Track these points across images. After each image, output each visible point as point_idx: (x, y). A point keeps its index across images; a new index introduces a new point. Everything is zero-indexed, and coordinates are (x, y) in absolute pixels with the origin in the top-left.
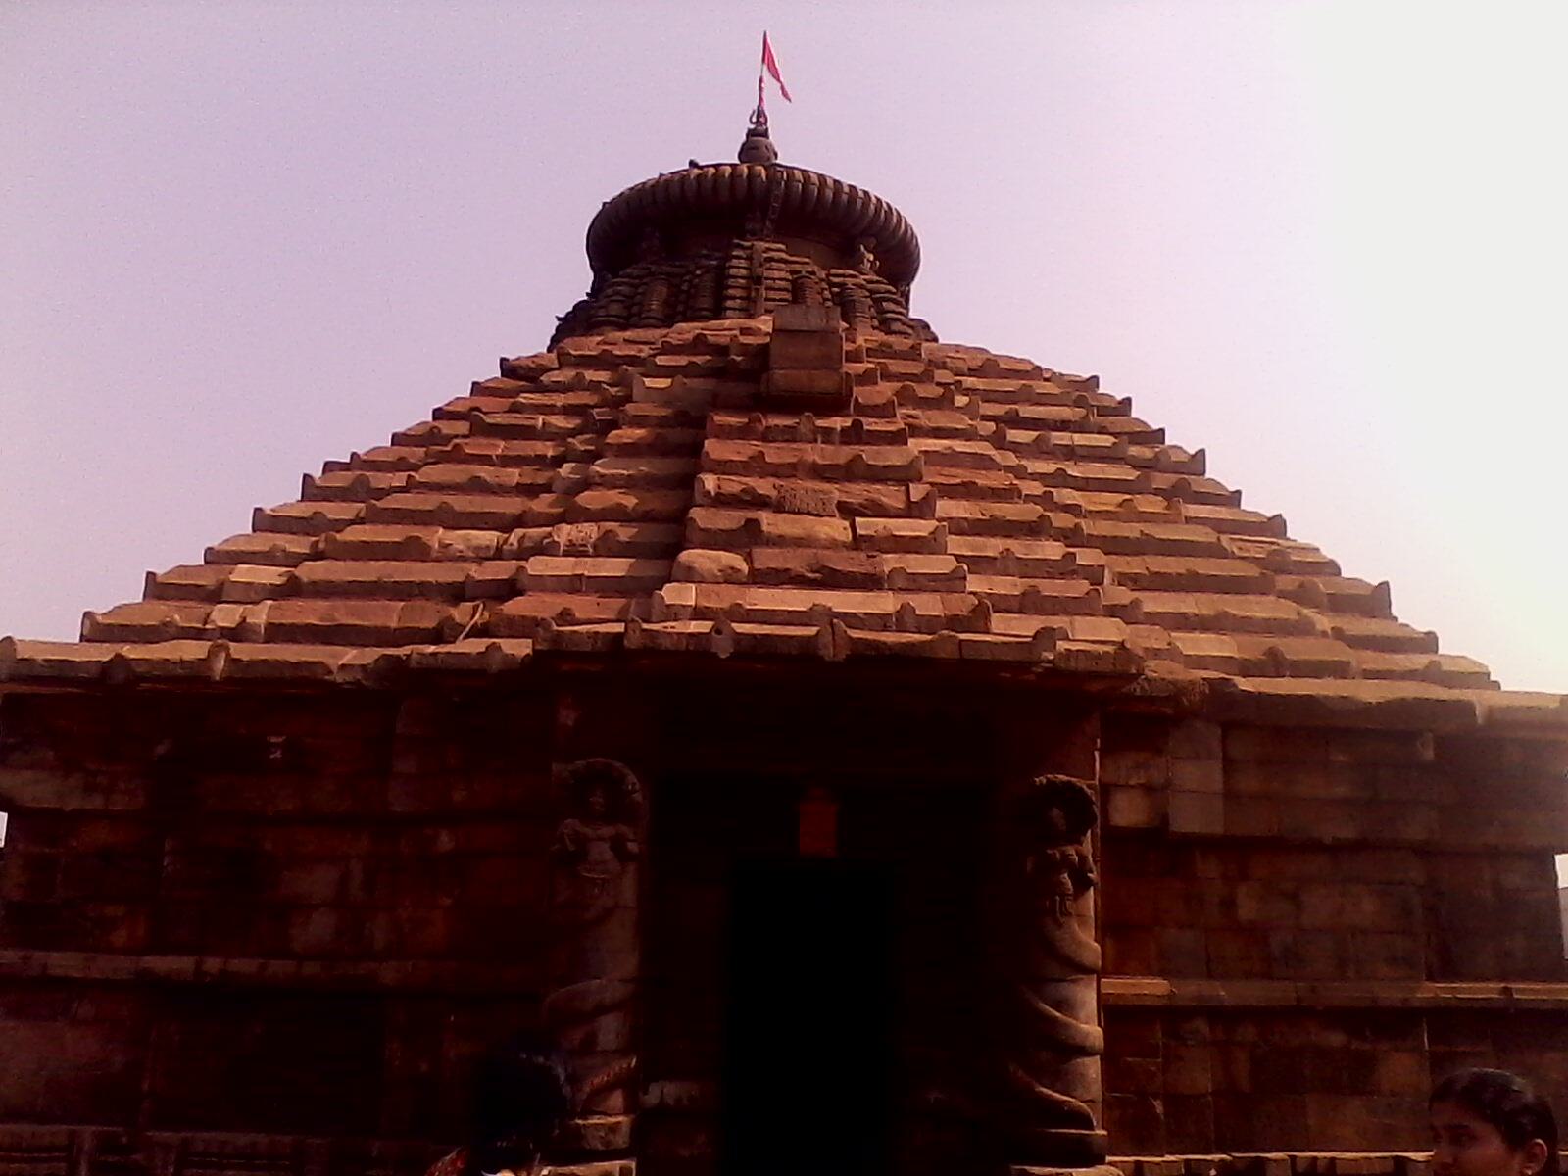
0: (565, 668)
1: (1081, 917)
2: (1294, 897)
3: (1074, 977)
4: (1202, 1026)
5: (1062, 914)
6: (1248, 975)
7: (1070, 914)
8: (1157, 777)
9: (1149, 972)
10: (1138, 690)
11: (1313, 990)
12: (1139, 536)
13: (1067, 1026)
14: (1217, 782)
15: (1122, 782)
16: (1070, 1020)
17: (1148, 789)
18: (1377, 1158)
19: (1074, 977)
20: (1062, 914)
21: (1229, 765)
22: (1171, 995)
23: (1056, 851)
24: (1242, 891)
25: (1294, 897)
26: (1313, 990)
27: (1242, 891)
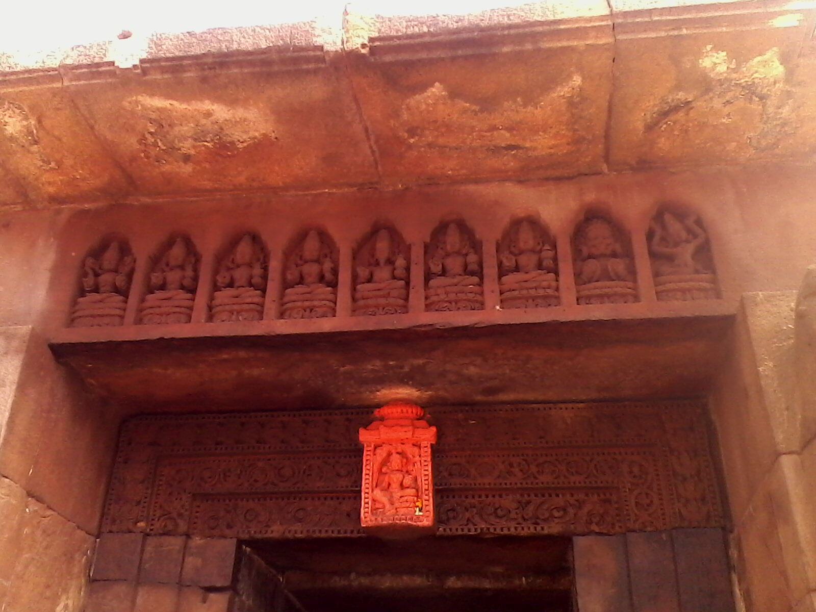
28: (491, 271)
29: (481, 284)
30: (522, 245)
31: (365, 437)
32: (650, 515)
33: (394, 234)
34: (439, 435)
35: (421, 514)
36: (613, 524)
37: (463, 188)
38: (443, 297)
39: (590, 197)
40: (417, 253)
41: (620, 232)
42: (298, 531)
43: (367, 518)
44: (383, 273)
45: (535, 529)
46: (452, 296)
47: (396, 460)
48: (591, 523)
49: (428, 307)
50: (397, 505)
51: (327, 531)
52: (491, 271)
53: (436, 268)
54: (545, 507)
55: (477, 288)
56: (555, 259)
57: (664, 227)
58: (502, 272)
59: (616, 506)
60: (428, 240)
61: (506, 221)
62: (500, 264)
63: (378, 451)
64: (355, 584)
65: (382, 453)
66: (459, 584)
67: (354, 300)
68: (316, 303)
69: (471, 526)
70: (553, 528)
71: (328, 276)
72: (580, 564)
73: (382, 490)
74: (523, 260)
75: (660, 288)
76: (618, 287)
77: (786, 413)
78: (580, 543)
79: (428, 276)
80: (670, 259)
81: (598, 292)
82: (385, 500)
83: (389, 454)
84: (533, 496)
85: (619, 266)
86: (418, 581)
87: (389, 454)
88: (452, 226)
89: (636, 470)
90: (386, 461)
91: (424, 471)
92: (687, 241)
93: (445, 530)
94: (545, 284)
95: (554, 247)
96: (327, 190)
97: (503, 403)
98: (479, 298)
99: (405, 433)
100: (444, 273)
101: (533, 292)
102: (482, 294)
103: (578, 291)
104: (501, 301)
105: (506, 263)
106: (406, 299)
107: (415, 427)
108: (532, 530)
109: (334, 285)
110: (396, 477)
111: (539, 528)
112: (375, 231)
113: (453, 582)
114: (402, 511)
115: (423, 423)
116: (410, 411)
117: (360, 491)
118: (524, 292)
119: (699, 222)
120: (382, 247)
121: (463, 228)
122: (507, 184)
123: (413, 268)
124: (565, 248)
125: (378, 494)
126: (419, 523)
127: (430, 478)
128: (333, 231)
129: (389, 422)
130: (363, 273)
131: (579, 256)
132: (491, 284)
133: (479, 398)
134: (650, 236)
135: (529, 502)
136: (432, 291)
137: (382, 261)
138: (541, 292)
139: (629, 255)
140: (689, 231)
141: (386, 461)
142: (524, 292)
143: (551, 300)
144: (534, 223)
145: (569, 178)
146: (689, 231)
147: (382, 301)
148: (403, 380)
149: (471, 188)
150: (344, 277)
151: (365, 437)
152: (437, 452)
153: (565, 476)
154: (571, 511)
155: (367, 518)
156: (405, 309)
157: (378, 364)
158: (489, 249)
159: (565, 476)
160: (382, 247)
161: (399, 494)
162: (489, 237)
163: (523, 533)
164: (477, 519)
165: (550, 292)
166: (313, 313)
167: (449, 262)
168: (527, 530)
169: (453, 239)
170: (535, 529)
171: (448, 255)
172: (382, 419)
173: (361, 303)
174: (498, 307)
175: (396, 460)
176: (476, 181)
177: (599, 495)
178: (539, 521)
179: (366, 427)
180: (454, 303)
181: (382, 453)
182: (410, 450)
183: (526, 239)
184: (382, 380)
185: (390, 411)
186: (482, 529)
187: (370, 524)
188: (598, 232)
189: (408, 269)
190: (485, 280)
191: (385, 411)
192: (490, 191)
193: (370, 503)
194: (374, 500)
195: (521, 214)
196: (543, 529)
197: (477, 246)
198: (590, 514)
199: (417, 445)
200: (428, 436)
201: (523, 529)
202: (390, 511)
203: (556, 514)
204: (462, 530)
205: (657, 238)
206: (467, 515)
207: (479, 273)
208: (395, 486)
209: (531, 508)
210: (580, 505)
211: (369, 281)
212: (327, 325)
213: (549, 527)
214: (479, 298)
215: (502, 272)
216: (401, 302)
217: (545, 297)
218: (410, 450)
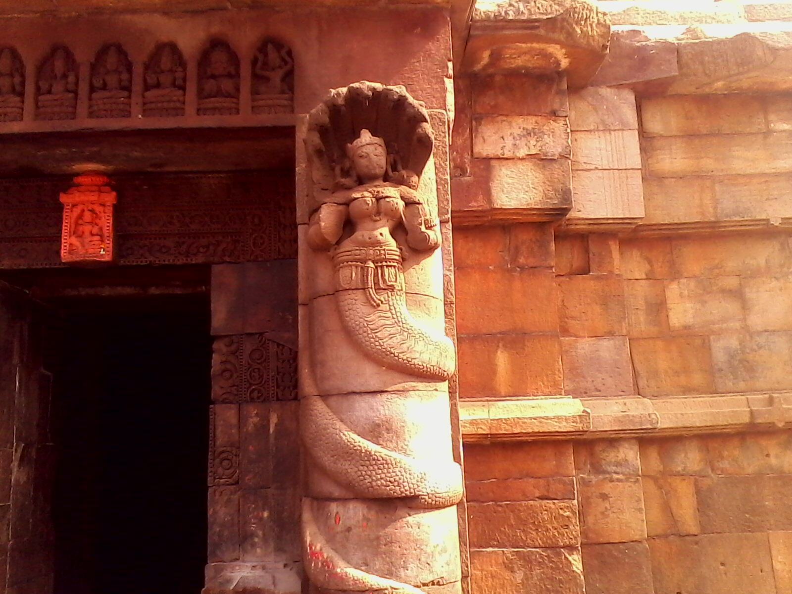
0: (178, 283)
1: (414, 297)
2: (738, 294)
3: (399, 387)
4: (630, 454)
5: (378, 289)
6: (687, 390)
7: (392, 288)
8: (553, 145)
9: (555, 391)
10: (511, 13)
11: (771, 401)
12: (723, 302)
13: (386, 463)
14: (635, 160)
15: (508, 154)
16: (394, 455)
17: (542, 160)
18: (460, 453)
19: (399, 387)
20: (378, 289)
21: (645, 137)
22: (584, 416)
23: (366, 194)
24: (673, 290)
25: (738, 294)
26: (771, 401)
27: (673, 290)
28: (137, 87)
29: (129, 97)
30: (162, 66)
31: (64, 198)
32: (261, 251)
33: (69, 56)
34: (120, 197)
35: (104, 253)
36: (239, 256)
37: (122, 17)
38: (102, 107)
39: (215, 29)
40: (84, 72)
41: (234, 59)
42: (22, 265)
43: (65, 256)
44: (58, 87)
45: (187, 260)
46: (107, 107)
47: (88, 216)
48: (225, 256)
49: (91, 115)
50: (87, 247)
51: (41, 264)
52: (137, 87)
53: (98, 83)
54: (195, 245)
55: (126, 101)
56: (184, 80)
57: (266, 55)
58: (147, 88)
59: (242, 244)
60: (93, 60)
61: (150, 47)
62: (145, 80)
63: (75, 209)
64: (83, 293)
65: (77, 211)
66: (157, 292)
67: (37, 107)
68: (8, 110)
69: (144, 260)
70: (200, 259)
71: (18, 88)
72: (214, 281)
73: (77, 237)
74: (163, 79)
75: (255, 103)
76: (227, 103)
77: (306, 198)
78: (216, 269)
79: (92, 89)
80: (267, 79)
81: (210, 106)
82: (78, 244)
83: (83, 211)
84: (187, 238)
85: (227, 85)
86: (128, 291)
87: (83, 211)
88: (113, 48)
89: (256, 220)
90: (81, 216)
91: (107, 222)
92: (280, 67)
93: (125, 262)
94: (175, 98)
95: (185, 70)
96: (16, 15)
97: (169, 173)
98: (127, 108)
99: (93, 197)
100: (104, 87)
101: (165, 105)
102: (130, 105)
103: (199, 104)
104: (144, 111)
105: (149, 81)
106: (75, 107)
107: (100, 191)
108: (185, 261)
109: (22, 94)
110: (87, 228)
111: (189, 259)
112: (55, 49)
113: (153, 291)
114: (91, 251)
115: (107, 188)
116: (98, 179)
117: (61, 237)
118: (159, 105)
119: (290, 53)
120: (59, 65)
121: (121, 51)
122: (155, 15)
123: (81, 83)
124: (192, 69)
125: (74, 240)
126: (103, 260)
127: (111, 229)
128: (21, 50)
129: (81, 188)
130: (44, 86)
131: (202, 77)
132: (136, 99)
133: (150, 169)
134: (254, 62)
135: (184, 243)
136: (94, 102)
137: (59, 75)
138: (172, 105)
139: (235, 76)
140: (283, 60)
141: (81, 216)
142: (159, 105)
143: (179, 111)
144: (173, 48)
145: (203, 12)
146: (283, 60)
147: (56, 109)
148: (90, 159)
149: (128, 17)
150: (30, 89)
151: (64, 198)
152: (118, 211)
153: (209, 225)
154: (211, 248)
155: (65, 256)
156: (73, 116)
157: (65, 151)
158: (138, 69)
159: (209, 225)
160: (59, 65)
161: (89, 239)
162: (139, 60)
163: (178, 263)
164: (147, 254)
165: (178, 105)
166: (7, 117)
167: (108, 79)
168: (181, 261)
169: (112, 60)
170: (187, 260)
171: (108, 73)
172: (79, 185)
173: (41, 110)
174: (140, 116)
175: (88, 216)
176: (134, 11)
177: (232, 237)
178: (189, 255)
179: (65, 191)
180: (109, 112)
181: (77, 211)
182: (98, 209)
183: (166, 62)
184: (73, 159)
185: (83, 180)
186: (150, 261)
187: (68, 260)
188: (219, 58)
189: (77, 84)
190: (132, 94)
191: (80, 180)
192: (140, 21)
193: (68, 246)
194: (71, 244)
195: (164, 39)
196: (192, 260)
197: (129, 67)
198: (224, 250)
199: (103, 205)
200: (110, 198)
201: (179, 260)
202: (82, 251)
203: (201, 250)
204: (137, 262)
205: (259, 64)
206: (141, 252)
207: (128, 89)
208: (87, 233)
209: (185, 246)
210: (219, 243)
211: (49, 92)
212: (16, 128)
213: (197, 259)
214: (127, 108)
215: (147, 88)
216: (70, 109)
217: (175, 109)
218: (98, 209)
